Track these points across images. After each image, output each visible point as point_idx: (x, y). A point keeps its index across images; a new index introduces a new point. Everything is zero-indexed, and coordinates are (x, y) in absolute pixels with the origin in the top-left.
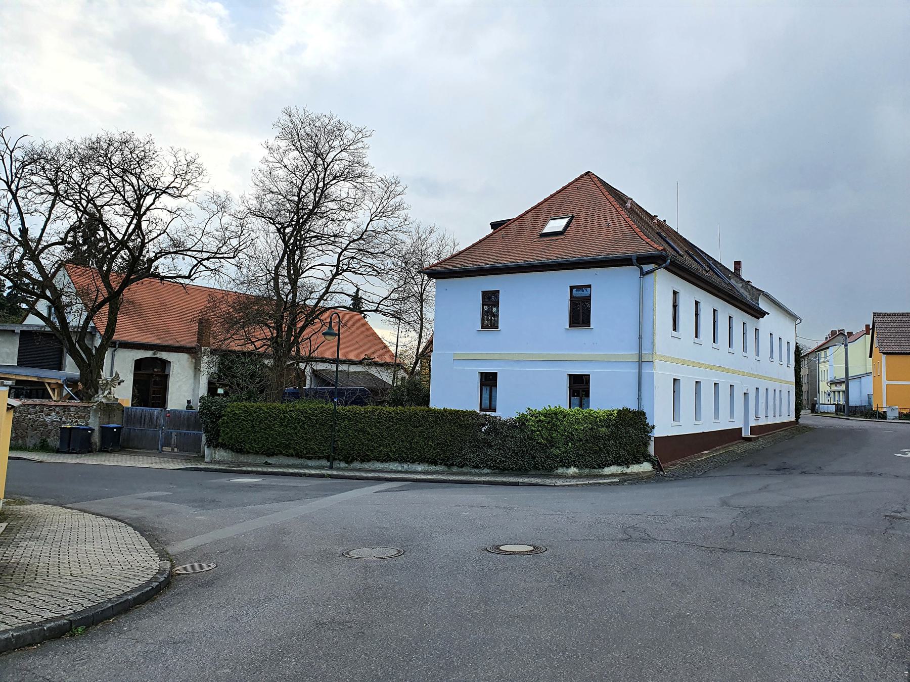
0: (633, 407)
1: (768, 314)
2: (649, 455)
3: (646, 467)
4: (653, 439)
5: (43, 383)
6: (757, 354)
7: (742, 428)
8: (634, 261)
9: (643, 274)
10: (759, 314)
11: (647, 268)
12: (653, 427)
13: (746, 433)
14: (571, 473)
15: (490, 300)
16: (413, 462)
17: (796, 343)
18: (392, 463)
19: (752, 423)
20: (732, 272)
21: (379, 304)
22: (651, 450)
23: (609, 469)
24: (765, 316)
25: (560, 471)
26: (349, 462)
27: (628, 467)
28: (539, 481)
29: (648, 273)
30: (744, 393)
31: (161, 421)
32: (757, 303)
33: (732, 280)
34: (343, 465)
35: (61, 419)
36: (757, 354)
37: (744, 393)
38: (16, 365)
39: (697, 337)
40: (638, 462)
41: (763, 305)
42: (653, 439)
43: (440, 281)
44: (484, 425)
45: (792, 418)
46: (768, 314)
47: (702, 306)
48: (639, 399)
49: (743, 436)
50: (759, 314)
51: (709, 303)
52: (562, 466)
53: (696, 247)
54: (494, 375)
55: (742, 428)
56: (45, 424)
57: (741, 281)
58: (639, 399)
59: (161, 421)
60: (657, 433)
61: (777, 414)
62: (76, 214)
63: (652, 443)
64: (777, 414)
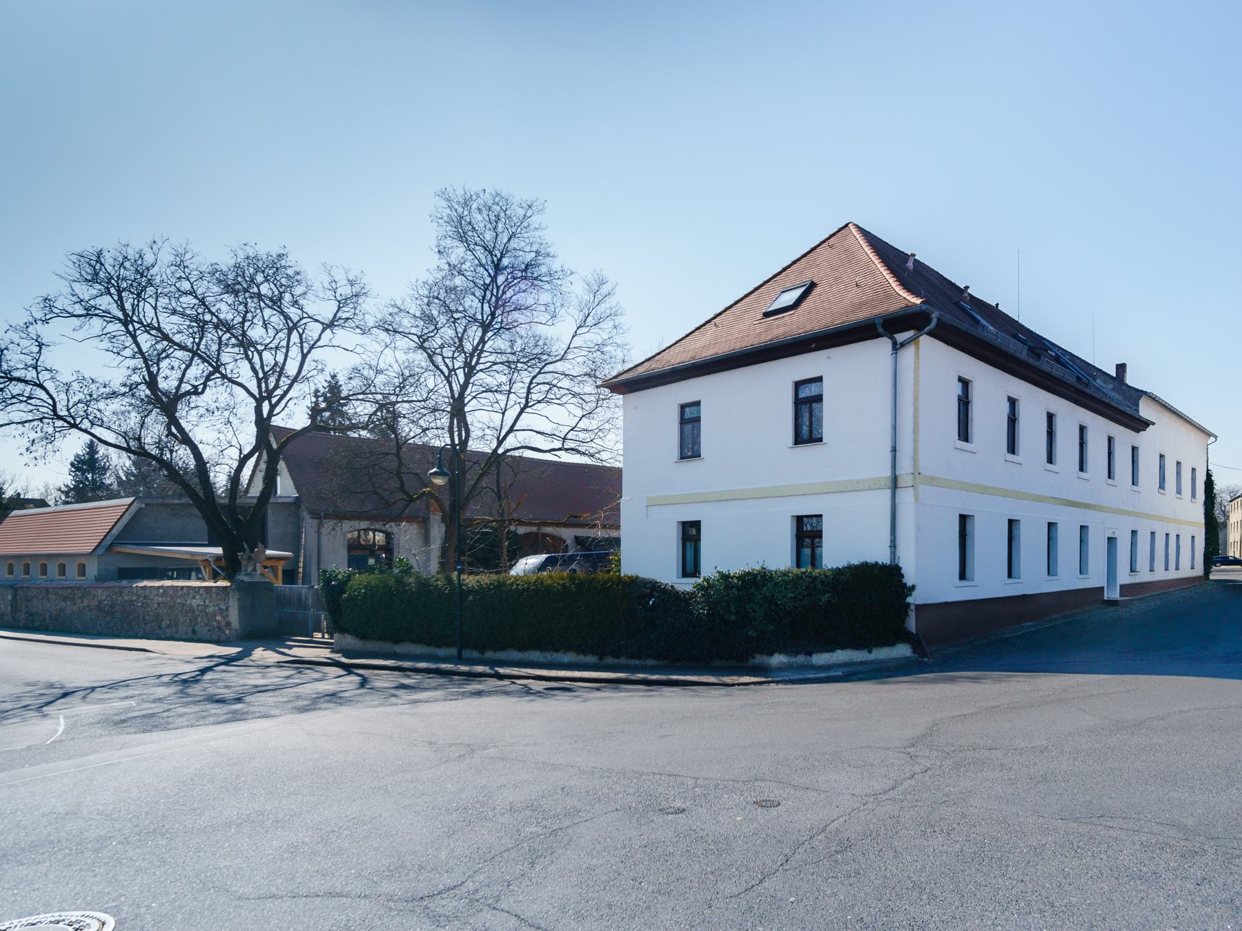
0: (883, 557)
1: (1153, 424)
2: (910, 633)
3: (902, 651)
4: (912, 607)
5: (196, 560)
6: (1134, 482)
7: (1103, 588)
8: (881, 330)
9: (897, 347)
10: (1140, 425)
11: (901, 337)
12: (913, 588)
13: (1115, 595)
14: (775, 663)
15: (689, 418)
16: (557, 651)
17: (1208, 470)
18: (532, 652)
19: (1124, 577)
20: (1112, 377)
21: (564, 439)
22: (911, 624)
23: (878, 656)
24: (1149, 428)
25: (759, 659)
26: (482, 651)
27: (870, 652)
28: (712, 679)
29: (903, 345)
30: (1109, 538)
31: (310, 602)
32: (1135, 410)
33: (1098, 381)
34: (475, 654)
35: (204, 602)
36: (1134, 482)
37: (1109, 538)
38: (207, 543)
39: (1013, 453)
40: (890, 643)
41: (1146, 410)
42: (912, 607)
43: (626, 395)
44: (651, 596)
45: (1199, 571)
46: (1153, 424)
47: (1090, 436)
48: (893, 546)
49: (1106, 598)
50: (1140, 425)
51: (1070, 415)
52: (761, 653)
53: (1045, 339)
54: (696, 525)
55: (1103, 588)
56: (191, 606)
57: (1111, 381)
58: (893, 546)
59: (310, 602)
60: (914, 599)
61: (1172, 565)
62: (246, 364)
63: (912, 614)
64: (1172, 565)
